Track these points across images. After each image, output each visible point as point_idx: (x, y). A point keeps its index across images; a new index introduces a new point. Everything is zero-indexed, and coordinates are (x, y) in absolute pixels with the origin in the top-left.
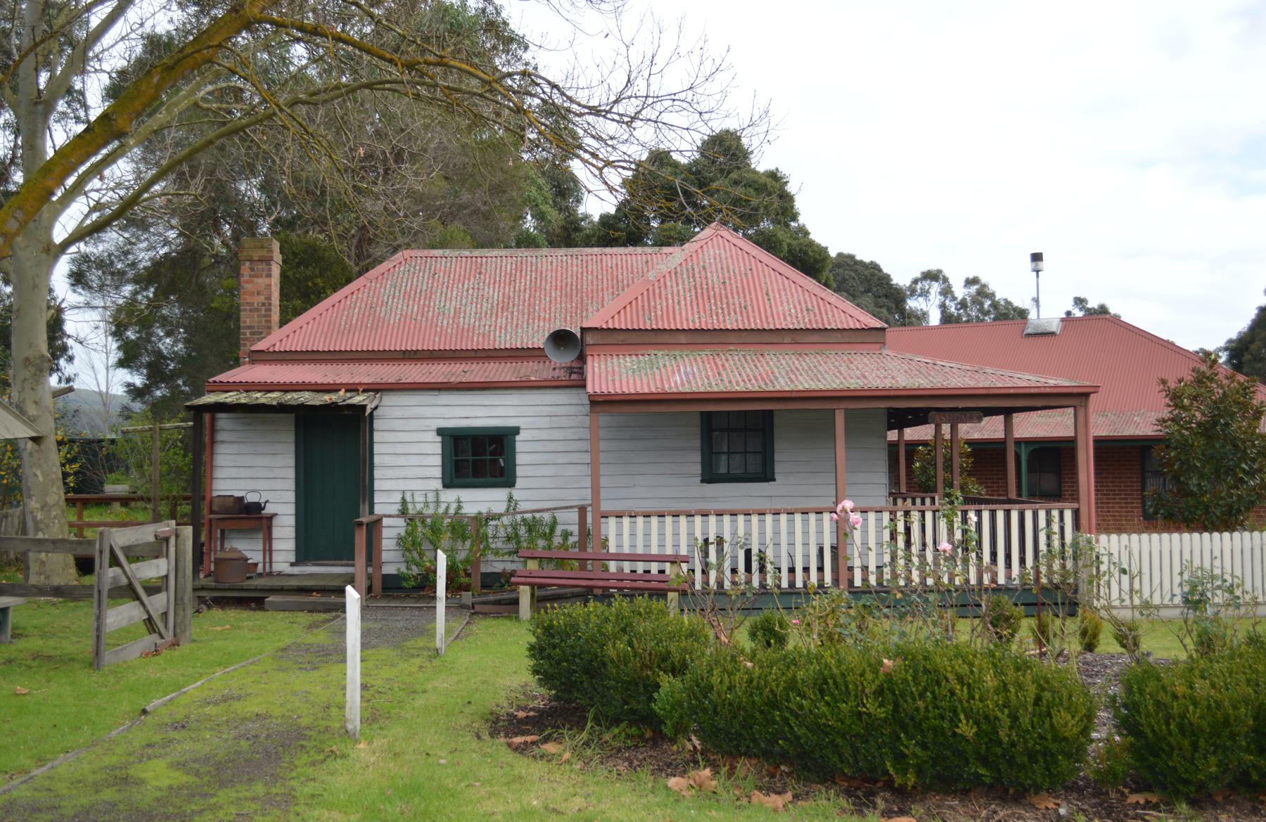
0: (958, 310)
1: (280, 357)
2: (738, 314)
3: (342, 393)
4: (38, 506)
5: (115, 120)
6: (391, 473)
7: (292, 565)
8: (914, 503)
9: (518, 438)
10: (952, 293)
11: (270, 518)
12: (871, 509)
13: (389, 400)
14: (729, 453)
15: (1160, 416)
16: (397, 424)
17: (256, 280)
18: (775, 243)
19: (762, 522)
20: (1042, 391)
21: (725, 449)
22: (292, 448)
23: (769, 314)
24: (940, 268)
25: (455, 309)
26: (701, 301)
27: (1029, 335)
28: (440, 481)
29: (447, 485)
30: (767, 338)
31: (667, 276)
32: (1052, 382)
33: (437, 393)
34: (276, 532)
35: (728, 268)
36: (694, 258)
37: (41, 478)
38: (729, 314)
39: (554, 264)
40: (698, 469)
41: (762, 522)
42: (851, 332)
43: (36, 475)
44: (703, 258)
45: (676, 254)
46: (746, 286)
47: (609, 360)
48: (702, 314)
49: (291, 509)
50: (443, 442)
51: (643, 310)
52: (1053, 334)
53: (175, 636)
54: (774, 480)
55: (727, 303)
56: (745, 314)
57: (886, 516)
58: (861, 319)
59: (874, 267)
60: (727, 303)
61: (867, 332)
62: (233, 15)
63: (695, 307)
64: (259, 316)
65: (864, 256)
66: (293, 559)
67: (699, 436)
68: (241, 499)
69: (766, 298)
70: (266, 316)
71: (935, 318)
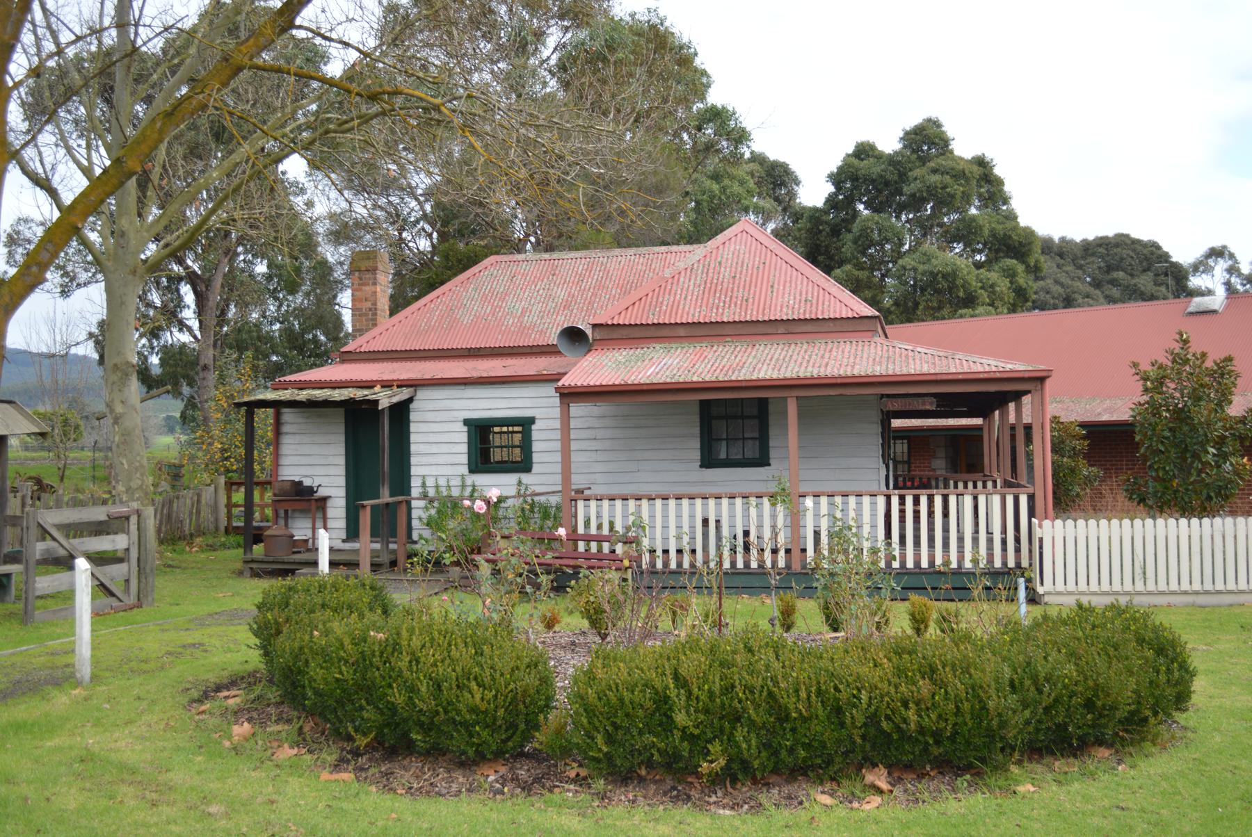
0: (1244, 285)
1: (365, 356)
2: (738, 306)
3: (378, 388)
4: (124, 489)
5: (125, 162)
6: (424, 460)
7: (344, 541)
8: (966, 487)
9: (534, 427)
10: (1238, 270)
11: (324, 499)
12: (823, 494)
13: (422, 394)
14: (727, 439)
15: (1136, 400)
16: (430, 416)
17: (364, 288)
18: (975, 228)
19: (732, 505)
20: (992, 375)
21: (724, 436)
22: (342, 438)
23: (767, 306)
24: (1224, 243)
25: (523, 309)
26: (706, 295)
27: (1191, 313)
28: (466, 467)
29: (471, 471)
30: (761, 329)
31: (683, 273)
32: (1009, 367)
33: (463, 387)
34: (330, 513)
35: (743, 263)
36: (714, 254)
37: (126, 466)
38: (730, 306)
39: (622, 263)
40: (697, 455)
41: (732, 505)
42: (843, 321)
43: (122, 464)
44: (722, 255)
45: (698, 251)
46: (754, 280)
47: (866, 348)
48: (704, 308)
49: (342, 492)
50: (469, 432)
51: (650, 305)
52: (1214, 312)
53: (139, 600)
54: (769, 465)
55: (731, 297)
56: (744, 306)
57: (881, 501)
58: (855, 308)
59: (1155, 246)
60: (731, 297)
61: (859, 321)
62: (224, 64)
63: (700, 301)
64: (367, 320)
65: (1141, 233)
66: (344, 537)
67: (698, 424)
68: (300, 483)
69: (770, 289)
70: (372, 320)
71: (1218, 299)
